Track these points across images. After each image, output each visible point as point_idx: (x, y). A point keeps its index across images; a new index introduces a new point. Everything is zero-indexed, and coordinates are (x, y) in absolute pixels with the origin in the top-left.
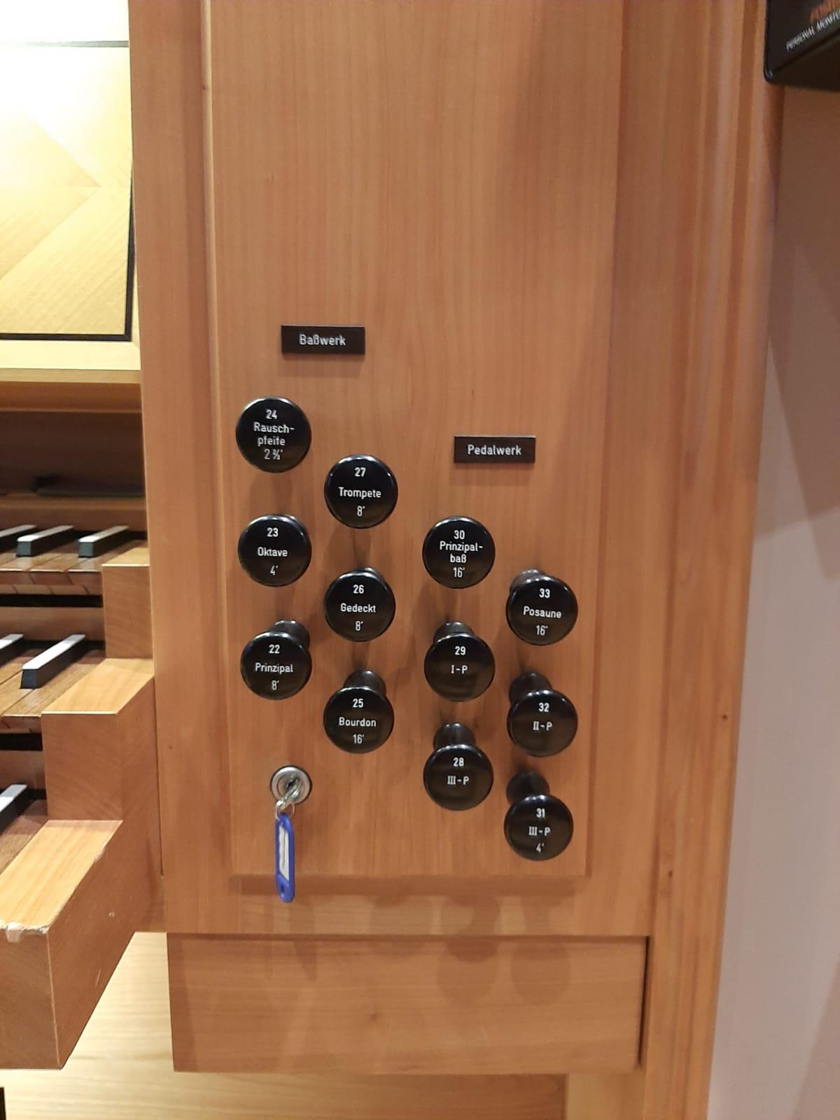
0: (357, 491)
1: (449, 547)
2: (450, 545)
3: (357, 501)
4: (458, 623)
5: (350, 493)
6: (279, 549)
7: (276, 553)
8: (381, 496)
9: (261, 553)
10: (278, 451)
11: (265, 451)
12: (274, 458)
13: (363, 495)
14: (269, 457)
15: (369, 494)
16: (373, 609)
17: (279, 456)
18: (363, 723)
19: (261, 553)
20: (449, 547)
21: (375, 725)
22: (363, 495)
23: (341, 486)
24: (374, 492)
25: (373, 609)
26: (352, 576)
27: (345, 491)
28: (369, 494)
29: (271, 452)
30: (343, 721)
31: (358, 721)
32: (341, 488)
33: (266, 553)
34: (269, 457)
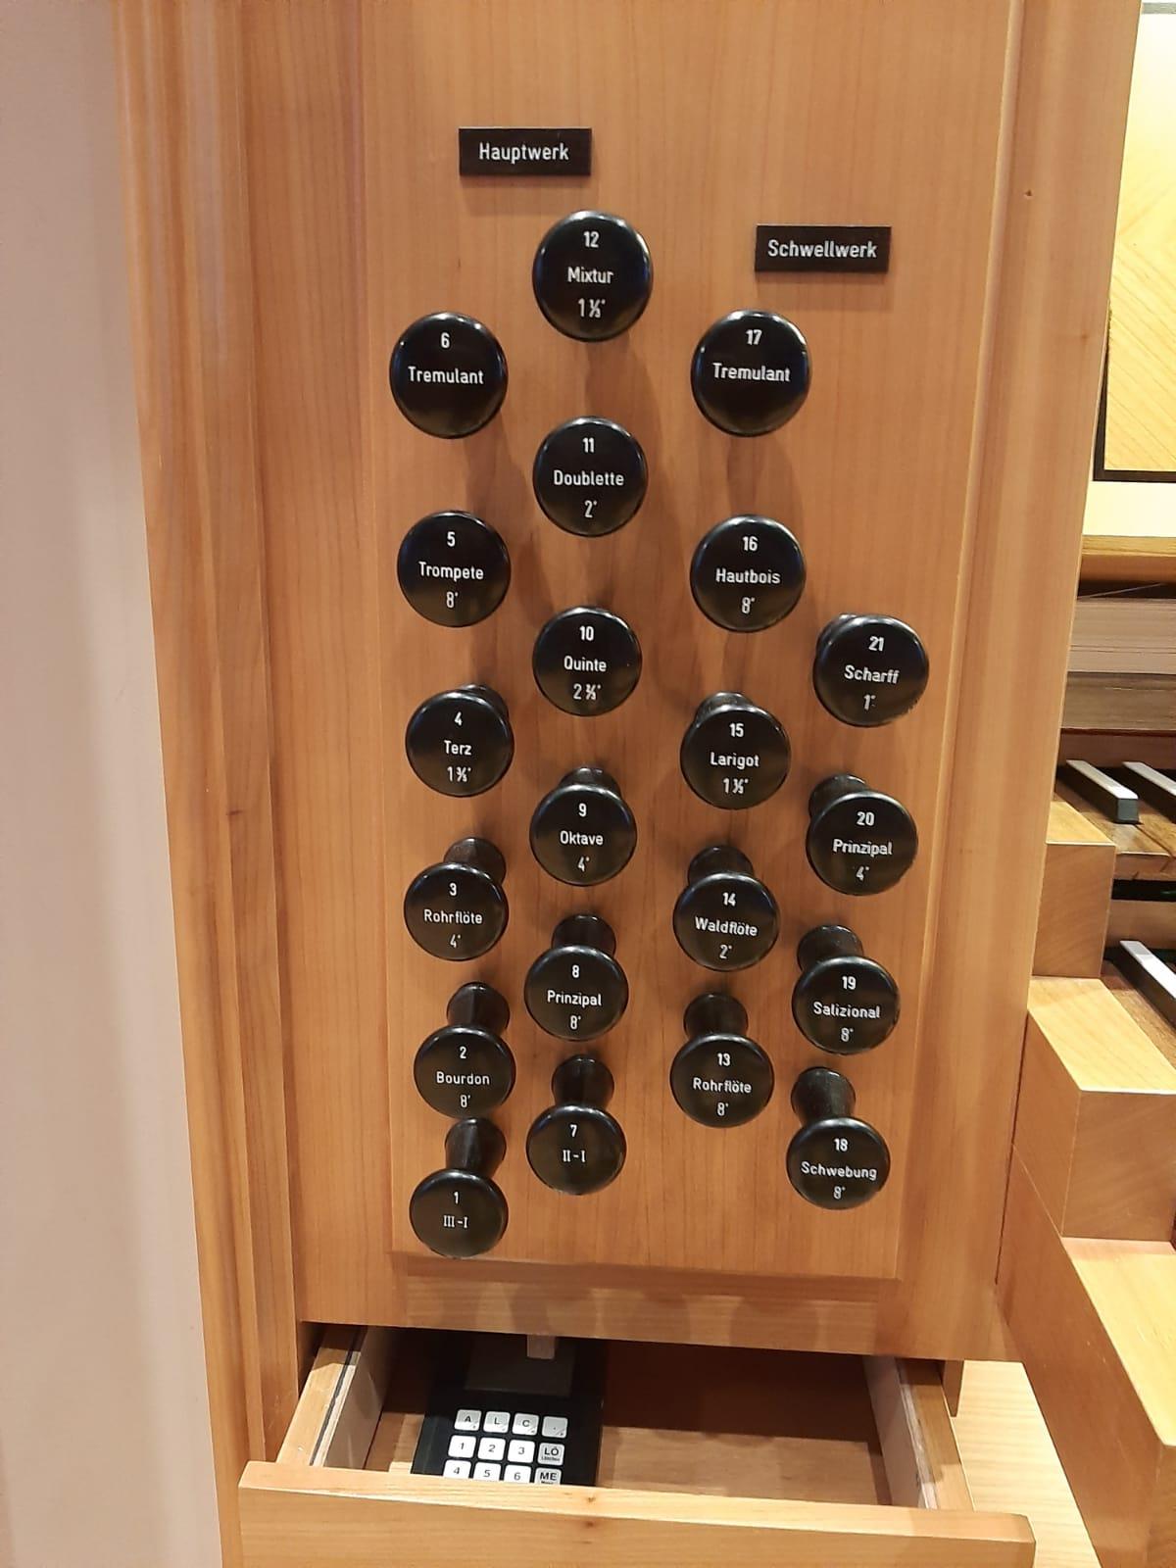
0: (447, 569)
1: (847, 847)
2: (850, 846)
3: (447, 583)
4: (584, 770)
5: (436, 572)
6: (589, 834)
7: (586, 839)
8: (607, 668)
9: (564, 839)
10: (594, 687)
11: (575, 687)
12: (588, 697)
13: (456, 574)
14: (579, 695)
15: (466, 574)
16: (576, 839)
17: (594, 694)
18: (471, 1080)
19: (564, 839)
20: (847, 847)
21: (488, 1082)
22: (456, 574)
23: (422, 561)
24: (473, 570)
25: (576, 839)
26: (458, 699)
27: (429, 568)
28: (466, 574)
29: (584, 688)
30: (442, 1077)
31: (463, 1077)
32: (423, 564)
33: (572, 839)
34: (579, 695)
